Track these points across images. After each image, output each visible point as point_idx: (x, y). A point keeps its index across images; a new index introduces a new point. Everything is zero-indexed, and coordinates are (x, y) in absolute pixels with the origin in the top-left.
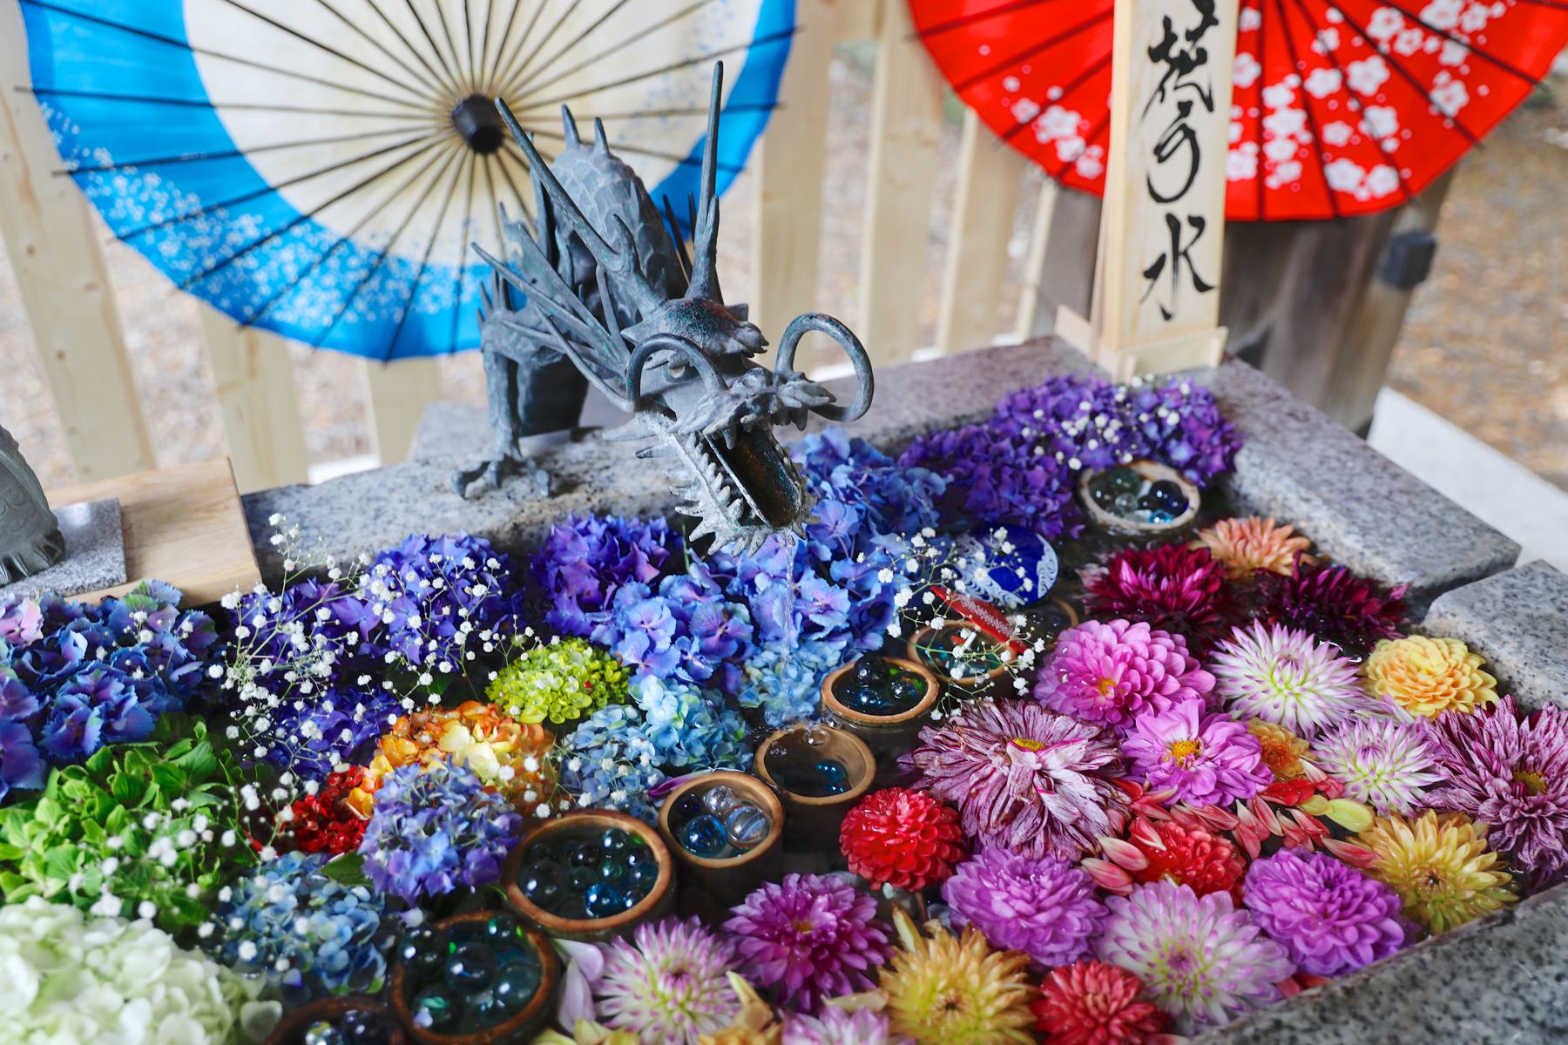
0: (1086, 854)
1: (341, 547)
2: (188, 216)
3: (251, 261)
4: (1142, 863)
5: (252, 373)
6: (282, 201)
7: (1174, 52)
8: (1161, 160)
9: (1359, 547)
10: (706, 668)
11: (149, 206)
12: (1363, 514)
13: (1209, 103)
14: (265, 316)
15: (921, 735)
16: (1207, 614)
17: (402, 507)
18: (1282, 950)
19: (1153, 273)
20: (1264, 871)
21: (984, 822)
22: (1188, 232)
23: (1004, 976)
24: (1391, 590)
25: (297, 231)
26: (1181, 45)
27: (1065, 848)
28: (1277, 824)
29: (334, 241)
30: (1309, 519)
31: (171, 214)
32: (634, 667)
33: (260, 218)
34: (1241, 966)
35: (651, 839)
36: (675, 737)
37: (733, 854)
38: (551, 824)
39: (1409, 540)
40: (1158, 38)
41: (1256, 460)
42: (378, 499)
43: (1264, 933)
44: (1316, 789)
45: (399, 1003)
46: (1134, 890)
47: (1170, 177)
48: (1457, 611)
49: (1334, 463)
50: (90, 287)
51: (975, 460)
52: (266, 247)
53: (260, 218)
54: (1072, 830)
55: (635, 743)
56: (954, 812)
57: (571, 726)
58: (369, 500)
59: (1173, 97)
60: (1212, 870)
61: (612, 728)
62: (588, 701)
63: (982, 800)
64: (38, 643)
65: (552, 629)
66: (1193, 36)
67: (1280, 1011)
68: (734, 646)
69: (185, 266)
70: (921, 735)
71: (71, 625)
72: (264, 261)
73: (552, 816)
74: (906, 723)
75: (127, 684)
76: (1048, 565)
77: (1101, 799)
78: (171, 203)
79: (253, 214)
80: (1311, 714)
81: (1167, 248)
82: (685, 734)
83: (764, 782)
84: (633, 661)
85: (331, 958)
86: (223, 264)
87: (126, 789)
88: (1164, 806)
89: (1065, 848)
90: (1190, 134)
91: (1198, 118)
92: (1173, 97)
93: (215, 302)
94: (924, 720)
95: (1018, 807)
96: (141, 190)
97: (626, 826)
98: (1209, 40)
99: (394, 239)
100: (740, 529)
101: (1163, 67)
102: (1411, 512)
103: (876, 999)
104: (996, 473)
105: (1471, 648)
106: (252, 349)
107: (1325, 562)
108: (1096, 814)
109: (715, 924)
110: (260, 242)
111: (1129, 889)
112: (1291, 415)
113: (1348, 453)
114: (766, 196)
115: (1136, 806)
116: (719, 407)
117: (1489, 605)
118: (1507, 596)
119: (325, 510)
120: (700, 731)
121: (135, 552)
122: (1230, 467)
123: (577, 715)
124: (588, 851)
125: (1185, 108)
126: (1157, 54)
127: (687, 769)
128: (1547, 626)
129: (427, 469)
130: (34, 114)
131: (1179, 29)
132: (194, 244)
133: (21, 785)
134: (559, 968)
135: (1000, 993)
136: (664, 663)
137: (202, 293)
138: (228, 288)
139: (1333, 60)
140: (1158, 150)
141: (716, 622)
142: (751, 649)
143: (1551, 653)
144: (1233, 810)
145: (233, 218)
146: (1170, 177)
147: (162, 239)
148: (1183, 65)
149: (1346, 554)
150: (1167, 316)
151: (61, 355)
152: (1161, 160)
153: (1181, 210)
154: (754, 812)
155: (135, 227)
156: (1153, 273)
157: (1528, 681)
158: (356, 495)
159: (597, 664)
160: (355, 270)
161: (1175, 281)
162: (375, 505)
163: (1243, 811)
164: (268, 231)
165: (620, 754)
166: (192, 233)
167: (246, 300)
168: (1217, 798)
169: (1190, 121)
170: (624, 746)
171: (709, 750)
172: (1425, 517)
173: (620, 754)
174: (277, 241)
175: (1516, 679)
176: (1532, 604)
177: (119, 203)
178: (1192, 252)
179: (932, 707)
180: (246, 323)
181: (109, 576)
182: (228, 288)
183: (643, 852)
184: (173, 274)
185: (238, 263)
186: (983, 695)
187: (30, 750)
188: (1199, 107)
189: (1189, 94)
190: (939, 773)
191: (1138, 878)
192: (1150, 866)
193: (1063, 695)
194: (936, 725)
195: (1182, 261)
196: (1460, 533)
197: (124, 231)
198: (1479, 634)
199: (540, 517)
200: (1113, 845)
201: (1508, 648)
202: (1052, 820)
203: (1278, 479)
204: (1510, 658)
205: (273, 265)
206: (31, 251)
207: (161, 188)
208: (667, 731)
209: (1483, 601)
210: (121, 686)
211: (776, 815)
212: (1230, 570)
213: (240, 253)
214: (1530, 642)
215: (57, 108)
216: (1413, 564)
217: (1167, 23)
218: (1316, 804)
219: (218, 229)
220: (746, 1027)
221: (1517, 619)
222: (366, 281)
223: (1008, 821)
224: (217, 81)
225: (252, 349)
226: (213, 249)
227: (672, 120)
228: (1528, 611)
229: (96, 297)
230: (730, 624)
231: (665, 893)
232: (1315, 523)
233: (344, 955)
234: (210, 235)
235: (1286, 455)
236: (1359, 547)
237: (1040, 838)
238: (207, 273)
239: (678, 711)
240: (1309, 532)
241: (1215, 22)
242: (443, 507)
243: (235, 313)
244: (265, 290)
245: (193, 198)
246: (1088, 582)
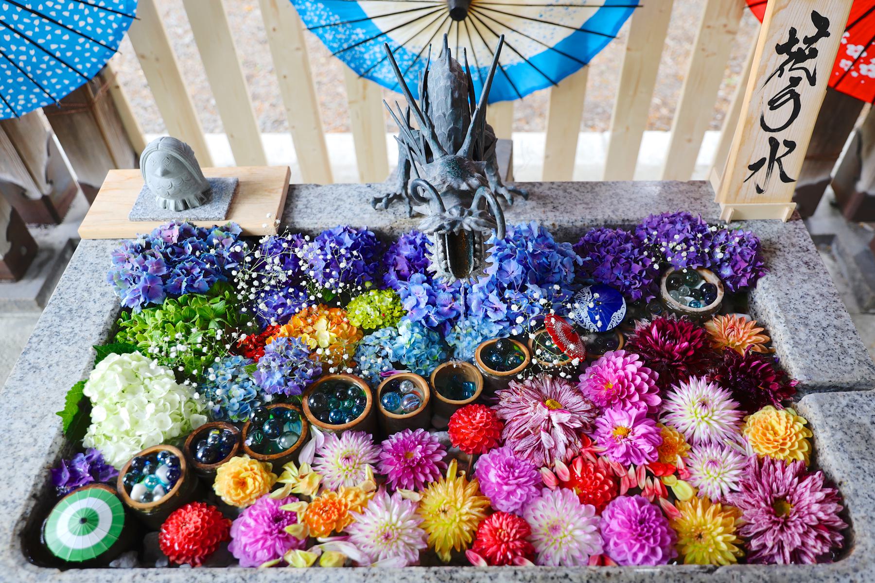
0: (545, 465)
1: (316, 221)
2: (335, 25)
3: (361, 48)
4: (567, 478)
5: (364, 98)
6: (373, 24)
7: (794, 49)
8: (772, 108)
9: (788, 352)
10: (435, 321)
11: (320, 17)
12: (803, 334)
13: (812, 80)
14: (370, 74)
15: (510, 384)
16: (679, 365)
17: (348, 206)
18: (601, 542)
19: (755, 167)
20: (621, 503)
21: (510, 435)
22: (782, 150)
23: (473, 507)
24: (791, 380)
25: (380, 39)
26: (801, 45)
27: (538, 458)
28: (644, 482)
29: (396, 46)
30: (774, 327)
31: (328, 22)
32: (407, 312)
33: (364, 31)
34: (578, 542)
35: (368, 395)
36: (404, 351)
37: (402, 413)
38: (334, 376)
39: (817, 357)
40: (785, 39)
41: (766, 286)
42: (341, 200)
43: (599, 531)
44: (677, 473)
45: (244, 432)
46: (556, 489)
47: (777, 118)
48: (813, 405)
49: (809, 300)
50: (298, 49)
51: (608, 252)
52: (368, 44)
53: (364, 31)
54: (547, 452)
55: (387, 349)
56: (502, 423)
57: (370, 332)
58: (338, 199)
59: (787, 75)
60: (595, 494)
61: (383, 339)
62: (381, 322)
63: (514, 424)
64: (175, 244)
65: (382, 285)
66: (808, 41)
67: (572, 571)
68: (454, 314)
69: (335, 45)
70: (510, 384)
71: (188, 240)
72: (368, 50)
73: (335, 373)
74: (503, 377)
75: (202, 270)
76: (619, 315)
77: (567, 442)
78: (328, 17)
79: (362, 28)
80: (701, 433)
81: (767, 156)
82: (409, 351)
83: (430, 385)
84: (408, 309)
85: (234, 404)
86: (350, 48)
87: (188, 314)
88: (597, 455)
89: (538, 458)
90: (796, 97)
91: (803, 88)
92: (787, 75)
93: (348, 64)
94: (514, 377)
95: (528, 434)
96: (317, 9)
97: (362, 386)
98: (820, 45)
100: (445, 273)
101: (785, 57)
102: (831, 341)
103: (417, 497)
104: (617, 259)
105: (808, 426)
106: (365, 87)
107: (772, 353)
108: (561, 448)
109: (377, 442)
110: (365, 41)
111: (554, 488)
112: (806, 263)
113: (822, 295)
114: (628, 49)
115: (583, 450)
116: (433, 222)
117: (833, 407)
118: (847, 406)
119: (318, 201)
120: (416, 352)
121: (235, 205)
122: (753, 284)
123: (374, 327)
124: (342, 393)
125: (795, 81)
126: (780, 49)
127: (404, 367)
128: (857, 429)
129: (369, 189)
131: (800, 36)
132: (339, 36)
133: (153, 302)
134: (309, 437)
135: (467, 513)
136: (419, 314)
137: (342, 58)
138: (354, 59)
141: (448, 302)
142: (462, 317)
143: (846, 446)
144: (627, 468)
145: (354, 29)
147: (326, 32)
148: (800, 57)
149: (781, 353)
150: (759, 191)
151: (285, 77)
152: (772, 108)
153: (780, 137)
154: (415, 396)
155: (315, 25)
156: (755, 167)
157: (825, 454)
158: (334, 196)
159: (392, 306)
160: (408, 60)
161: (768, 175)
162: (339, 203)
163: (632, 470)
164: (368, 37)
165: (380, 352)
166: (337, 32)
167: (361, 65)
168: (622, 460)
169: (797, 89)
170: (383, 349)
171: (417, 361)
172: (837, 346)
173: (380, 352)
174: (372, 42)
175: (821, 451)
176: (858, 415)
177: (308, 13)
178: (782, 159)
179: (519, 372)
180: (361, 76)
181: (219, 216)
182: (354, 59)
183: (363, 399)
184: (331, 48)
185: (356, 48)
186: (548, 373)
187: (161, 288)
188: (805, 81)
189: (801, 74)
190: (506, 404)
191: (561, 484)
192: (570, 481)
193: (587, 383)
194: (518, 381)
195: (776, 164)
196: (850, 361)
197: (311, 26)
198: (816, 422)
199: (403, 226)
200: (560, 466)
201: (825, 435)
202: (540, 444)
203: (771, 301)
204: (823, 441)
205: (371, 52)
206: (274, 30)
207: (324, 9)
208: (402, 348)
209: (831, 405)
210: (199, 270)
211: (425, 402)
212: (715, 343)
213: (358, 44)
214: (839, 435)
216: (808, 370)
217: (793, 32)
218: (670, 480)
219: (348, 33)
220: (362, 489)
221: (843, 420)
222: (412, 66)
223: (520, 438)
225: (365, 87)
226: (346, 40)
227: (571, 8)
228: (853, 418)
229: (300, 53)
230: (455, 303)
231: (361, 422)
232: (775, 330)
233: (237, 405)
234: (344, 34)
235: (785, 287)
236: (788, 352)
237: (529, 451)
238: (344, 50)
239: (410, 340)
240: (772, 334)
241: (828, 35)
242: (364, 211)
243: (357, 70)
244: (369, 63)
245: (337, 17)
246: (638, 328)
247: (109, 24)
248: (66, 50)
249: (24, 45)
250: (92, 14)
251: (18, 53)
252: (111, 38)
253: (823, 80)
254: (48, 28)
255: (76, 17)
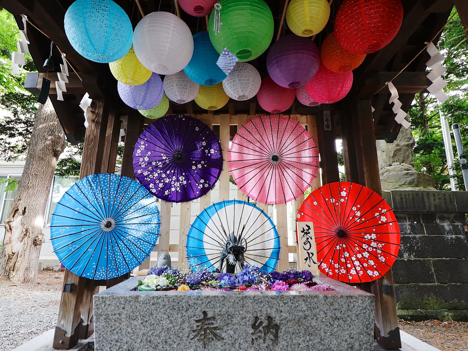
7: (305, 232)
47: (307, 246)
59: (305, 237)
66: (307, 230)
90: (309, 242)
99: (146, 94)
125: (308, 239)
126: (302, 232)
130: (185, 249)
139: (359, 252)
140: (304, 243)
146: (307, 246)
156: (306, 259)
188: (310, 239)
215: (188, 249)
217: (303, 228)
224: (205, 246)
247: (143, 255)
248: (129, 261)
249: (121, 257)
250: (140, 253)
251: (125, 252)
252: (141, 260)
253: (313, 238)
254: (129, 253)
255: (136, 252)
